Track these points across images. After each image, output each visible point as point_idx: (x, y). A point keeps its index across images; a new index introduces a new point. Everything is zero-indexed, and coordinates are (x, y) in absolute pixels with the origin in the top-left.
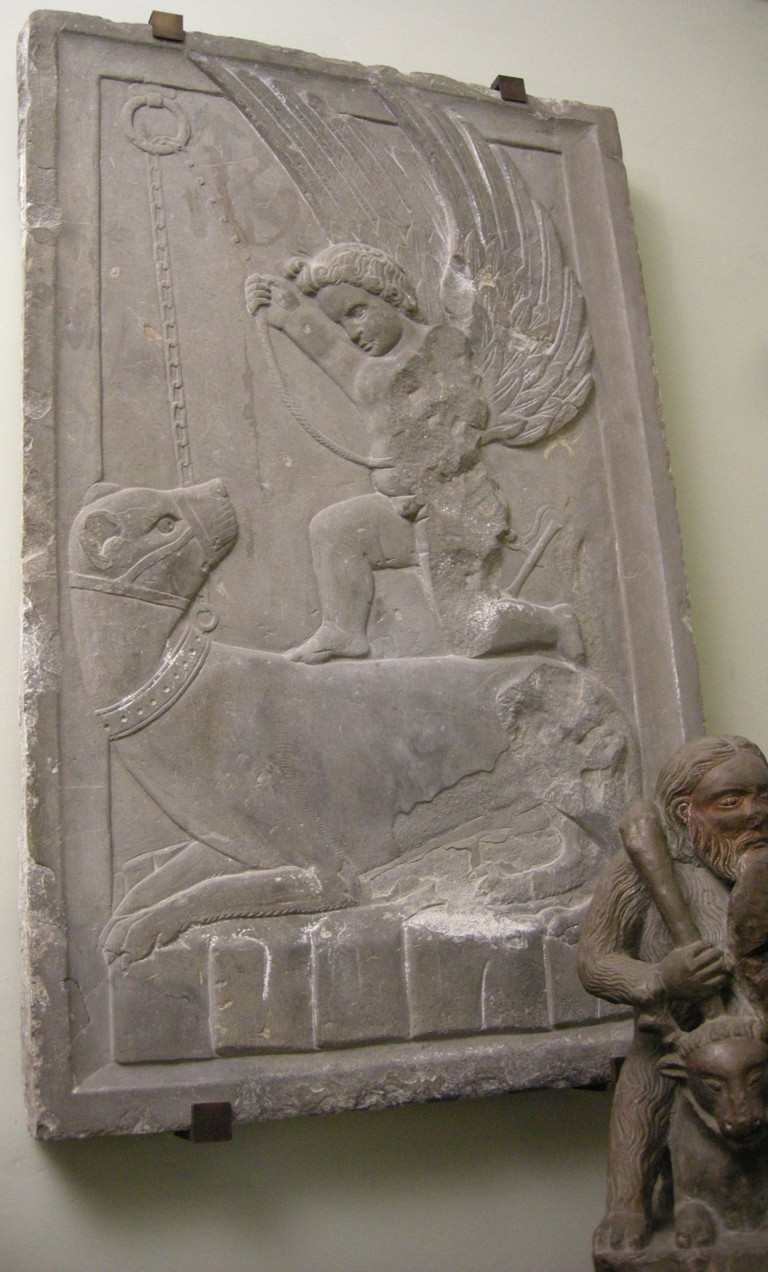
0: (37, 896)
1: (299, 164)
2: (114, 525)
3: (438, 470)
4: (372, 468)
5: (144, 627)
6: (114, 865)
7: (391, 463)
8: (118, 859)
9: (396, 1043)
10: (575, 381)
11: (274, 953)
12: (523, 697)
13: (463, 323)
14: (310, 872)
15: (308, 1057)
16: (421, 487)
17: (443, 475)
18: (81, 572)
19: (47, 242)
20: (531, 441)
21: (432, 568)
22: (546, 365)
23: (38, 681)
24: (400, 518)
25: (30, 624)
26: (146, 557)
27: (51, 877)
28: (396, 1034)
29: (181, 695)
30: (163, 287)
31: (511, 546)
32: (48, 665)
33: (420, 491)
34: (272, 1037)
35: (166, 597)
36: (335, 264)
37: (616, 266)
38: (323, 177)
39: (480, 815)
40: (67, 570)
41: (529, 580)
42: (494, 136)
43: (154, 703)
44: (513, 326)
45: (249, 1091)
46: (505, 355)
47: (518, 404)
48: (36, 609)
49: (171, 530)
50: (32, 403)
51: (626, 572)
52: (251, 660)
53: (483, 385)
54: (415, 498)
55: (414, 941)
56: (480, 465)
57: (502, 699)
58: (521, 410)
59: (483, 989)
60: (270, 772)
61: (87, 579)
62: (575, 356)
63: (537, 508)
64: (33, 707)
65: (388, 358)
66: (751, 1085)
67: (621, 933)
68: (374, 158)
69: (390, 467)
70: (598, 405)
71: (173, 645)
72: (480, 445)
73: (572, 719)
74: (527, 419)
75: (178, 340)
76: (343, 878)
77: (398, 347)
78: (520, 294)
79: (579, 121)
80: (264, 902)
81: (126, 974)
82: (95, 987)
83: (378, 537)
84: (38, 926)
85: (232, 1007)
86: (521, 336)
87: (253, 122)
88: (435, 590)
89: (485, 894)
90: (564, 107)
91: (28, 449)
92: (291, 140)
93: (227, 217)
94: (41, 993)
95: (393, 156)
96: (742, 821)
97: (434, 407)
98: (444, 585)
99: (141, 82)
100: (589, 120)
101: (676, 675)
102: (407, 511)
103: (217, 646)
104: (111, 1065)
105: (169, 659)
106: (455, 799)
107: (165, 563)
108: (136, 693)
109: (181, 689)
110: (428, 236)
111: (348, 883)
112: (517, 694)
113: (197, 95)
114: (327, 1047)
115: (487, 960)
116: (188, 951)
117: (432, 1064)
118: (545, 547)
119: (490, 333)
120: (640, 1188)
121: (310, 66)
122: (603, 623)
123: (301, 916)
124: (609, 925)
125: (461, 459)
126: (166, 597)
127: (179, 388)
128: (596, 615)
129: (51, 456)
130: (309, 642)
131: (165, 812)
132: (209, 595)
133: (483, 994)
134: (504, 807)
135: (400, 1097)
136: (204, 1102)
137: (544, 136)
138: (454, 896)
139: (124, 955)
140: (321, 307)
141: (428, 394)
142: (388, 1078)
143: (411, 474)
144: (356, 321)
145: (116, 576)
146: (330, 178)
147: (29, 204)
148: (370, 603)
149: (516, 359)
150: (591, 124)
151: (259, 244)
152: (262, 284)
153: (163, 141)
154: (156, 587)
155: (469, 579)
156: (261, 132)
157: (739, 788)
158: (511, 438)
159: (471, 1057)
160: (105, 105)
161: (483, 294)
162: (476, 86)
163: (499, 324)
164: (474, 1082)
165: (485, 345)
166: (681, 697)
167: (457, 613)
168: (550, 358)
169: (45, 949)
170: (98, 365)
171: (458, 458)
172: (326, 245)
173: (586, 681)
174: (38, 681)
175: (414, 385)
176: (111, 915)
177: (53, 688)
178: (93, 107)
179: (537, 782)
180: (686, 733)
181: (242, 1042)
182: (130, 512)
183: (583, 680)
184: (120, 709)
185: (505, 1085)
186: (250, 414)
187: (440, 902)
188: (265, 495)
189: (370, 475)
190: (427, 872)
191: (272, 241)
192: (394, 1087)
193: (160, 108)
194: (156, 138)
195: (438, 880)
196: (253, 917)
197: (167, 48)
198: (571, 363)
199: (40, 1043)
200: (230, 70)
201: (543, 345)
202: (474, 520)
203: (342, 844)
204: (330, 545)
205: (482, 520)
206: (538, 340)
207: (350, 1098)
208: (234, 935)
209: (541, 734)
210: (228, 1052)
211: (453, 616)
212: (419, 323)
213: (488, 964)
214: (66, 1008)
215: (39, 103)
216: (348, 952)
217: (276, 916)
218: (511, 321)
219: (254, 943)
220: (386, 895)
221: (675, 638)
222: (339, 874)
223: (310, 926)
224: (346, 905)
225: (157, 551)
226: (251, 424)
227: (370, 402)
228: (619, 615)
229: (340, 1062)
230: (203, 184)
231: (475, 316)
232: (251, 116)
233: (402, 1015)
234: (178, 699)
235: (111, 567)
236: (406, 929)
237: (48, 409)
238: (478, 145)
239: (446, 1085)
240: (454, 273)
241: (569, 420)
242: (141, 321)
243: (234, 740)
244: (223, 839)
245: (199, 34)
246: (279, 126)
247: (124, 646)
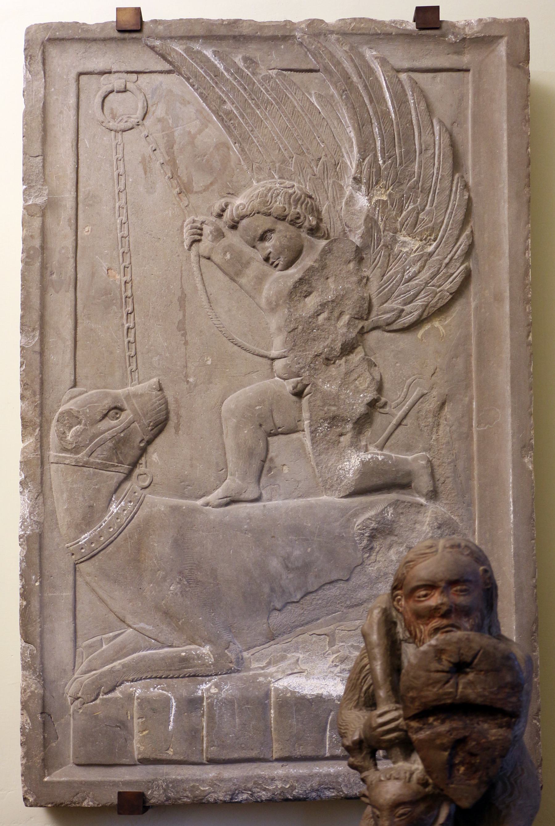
0: (25, 662)
1: (230, 120)
2: (77, 418)
3: (323, 356)
4: (273, 359)
5: (97, 487)
6: (77, 644)
7: (285, 354)
8: (79, 641)
9: (263, 762)
10: (451, 271)
11: (177, 701)
12: (376, 525)
13: (356, 234)
14: (206, 650)
15: (201, 767)
16: (308, 370)
17: (327, 359)
18: (57, 452)
19: (36, 214)
20: (406, 325)
21: (312, 432)
22: (426, 261)
23: (27, 527)
24: (291, 395)
25: (24, 489)
26: (98, 439)
27: (34, 651)
28: (262, 757)
29: (120, 533)
30: (122, 237)
31: (381, 410)
32: (34, 516)
33: (307, 373)
34: (175, 754)
35: (113, 466)
36: (253, 199)
37: (505, 165)
38: (250, 128)
39: (338, 611)
40: (49, 451)
41: (393, 436)
42: (406, 65)
43: (102, 539)
44: (401, 232)
45: (158, 786)
46: (391, 256)
47: (397, 296)
48: (27, 479)
49: (117, 418)
50: (26, 336)
51: (479, 424)
52: (171, 507)
53: (369, 284)
54: (302, 380)
55: (277, 697)
56: (360, 349)
57: (359, 527)
58: (399, 301)
59: (328, 730)
60: (179, 583)
61: (59, 456)
62: (454, 250)
63: (407, 379)
64: (24, 543)
65: (291, 271)
66: (398, 817)
67: (362, 695)
68: (296, 104)
69: (285, 357)
70: (473, 288)
71: (117, 499)
72: (362, 332)
73: (418, 540)
74: (405, 307)
75: (131, 277)
76: (229, 654)
77: (299, 261)
78: (410, 203)
79: (489, 36)
80: (173, 668)
81: (81, 711)
82: (62, 718)
83: (271, 411)
84: (26, 681)
85: (147, 734)
86: (407, 239)
87: (196, 90)
88: (313, 449)
89: (336, 666)
90: (477, 25)
91: (22, 369)
92: (227, 100)
93: (172, 174)
94: (27, 720)
95: (313, 100)
96: (430, 611)
97: (323, 305)
98: (322, 445)
99: (110, 73)
100: (497, 33)
101: (512, 504)
102: (295, 390)
103: (150, 498)
104: (71, 765)
105: (114, 509)
106: (318, 600)
107: (112, 441)
108: (90, 532)
109: (121, 529)
110: (336, 165)
111: (233, 657)
112: (371, 523)
113: (153, 76)
114: (212, 762)
115: (331, 711)
116: (121, 698)
117: (287, 777)
118: (410, 410)
119: (379, 239)
121: (246, 31)
122: (455, 466)
123: (199, 678)
124: (354, 689)
125: (342, 345)
126: (113, 466)
127: (131, 313)
128: (449, 460)
129: (38, 372)
130: (216, 492)
131: (111, 610)
132: (146, 462)
133: (328, 733)
134: (356, 605)
135: (263, 797)
136: (125, 790)
137: (455, 57)
138: (312, 667)
139: (80, 699)
140: (242, 237)
141: (320, 295)
142: (254, 784)
143: (300, 361)
144: (267, 244)
145: (79, 454)
146: (256, 127)
147: (25, 187)
148: (264, 461)
149: (400, 258)
150: (501, 37)
151: (196, 192)
152: (195, 224)
153: (125, 120)
154: (107, 459)
155: (342, 439)
156: (202, 97)
157: (428, 583)
158: (388, 324)
159: (316, 774)
160: (82, 96)
161: (376, 207)
162: (394, 22)
163: (388, 231)
164: (318, 790)
165: (374, 250)
166: (514, 521)
167: (329, 465)
168: (431, 255)
169: (29, 694)
170: (73, 303)
171: (340, 344)
172: (250, 185)
173: (432, 511)
174: (27, 527)
175: (309, 290)
176: (74, 674)
177: (37, 531)
178: (72, 101)
179: (386, 587)
180: (515, 548)
181: (154, 756)
182: (89, 407)
183: (430, 511)
184: (80, 543)
185: (341, 793)
186: (182, 327)
187: (301, 671)
188: (190, 387)
189: (272, 365)
190: (293, 650)
191: (206, 189)
192: (259, 790)
193: (125, 91)
194: (120, 118)
195: (301, 656)
196: (165, 678)
197: (129, 39)
198: (449, 256)
199: (25, 750)
200: (178, 48)
201: (426, 244)
202: (350, 392)
203: (230, 631)
204: (235, 420)
205: (357, 391)
206: (421, 240)
208: (152, 689)
209: (392, 551)
210: (145, 761)
211: (326, 467)
212: (319, 239)
213: (332, 713)
214: (42, 730)
215: (30, 104)
216: (229, 702)
217: (182, 677)
218: (399, 227)
219: (164, 694)
220: (262, 666)
221: (514, 475)
222: (226, 651)
223: (204, 685)
224: (230, 671)
225: (106, 433)
226: (182, 335)
227: (273, 308)
228: (470, 459)
229: (222, 772)
230: (155, 150)
231: (366, 227)
232: (194, 86)
233: (267, 743)
234: (118, 535)
235: (74, 447)
236: (273, 688)
237: (36, 339)
238: (388, 76)
239: (297, 791)
240: (353, 192)
241: (442, 305)
242: (105, 266)
243: (155, 562)
244: (148, 627)
245: (155, 22)
246: (217, 90)
247: (83, 501)
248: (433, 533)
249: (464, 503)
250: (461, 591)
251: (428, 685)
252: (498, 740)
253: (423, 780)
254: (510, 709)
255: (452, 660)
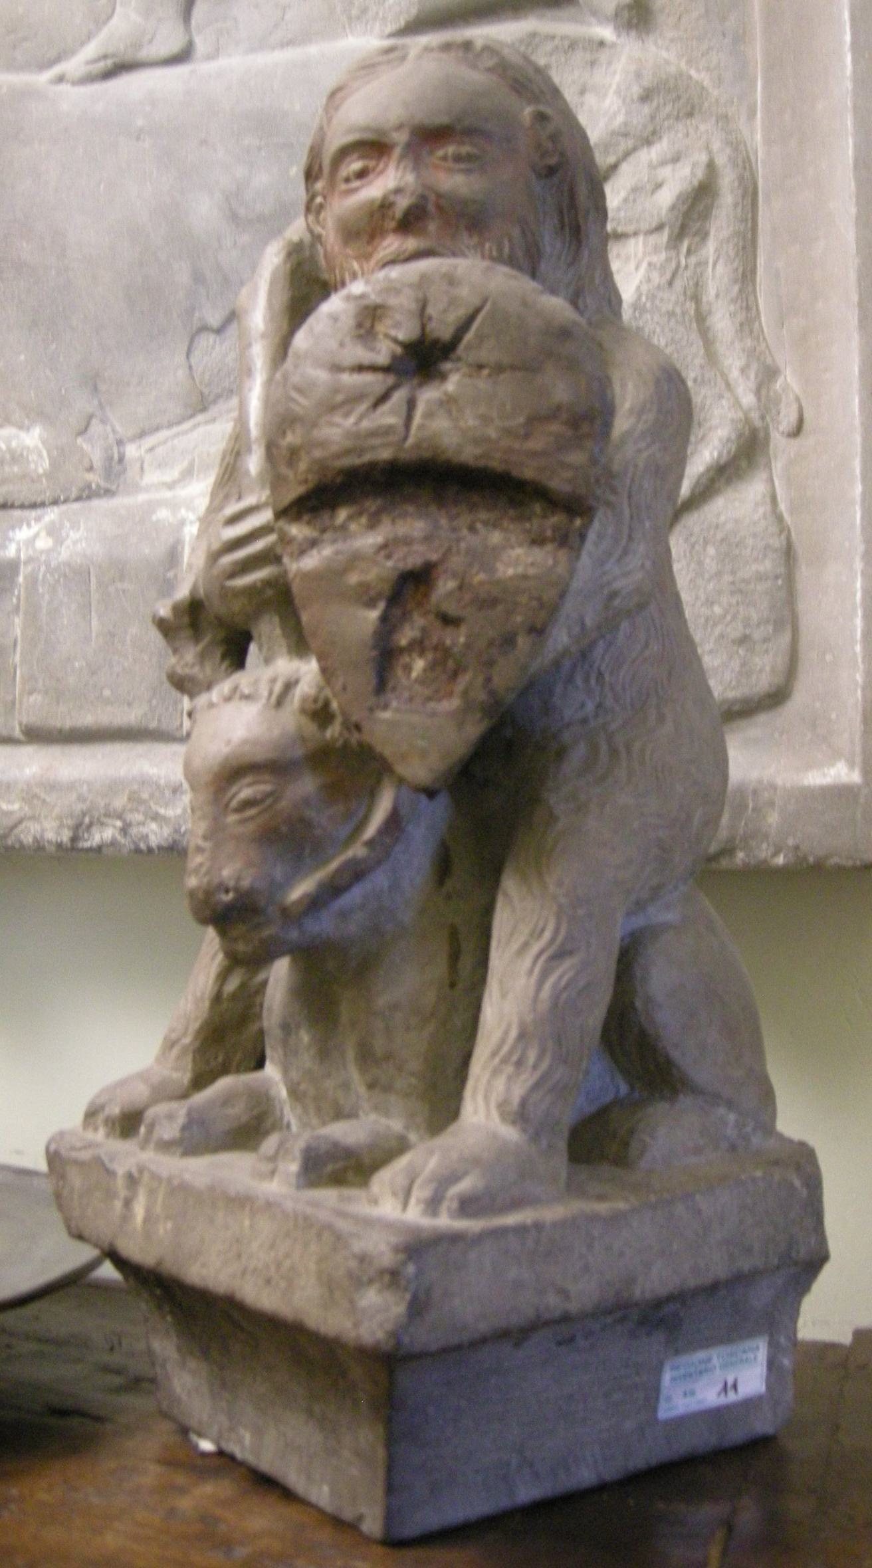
14: (32, 438)
28: (153, 725)
114: (37, 735)
120: (197, 1025)
142: (129, 799)
207: (61, 826)
220: (168, 478)
222: (80, 440)
224: (87, 494)
248: (628, 113)
249: (724, 35)
250: (458, 158)
251: (333, 408)
252: (525, 577)
253: (315, 700)
254: (566, 488)
255: (401, 336)
